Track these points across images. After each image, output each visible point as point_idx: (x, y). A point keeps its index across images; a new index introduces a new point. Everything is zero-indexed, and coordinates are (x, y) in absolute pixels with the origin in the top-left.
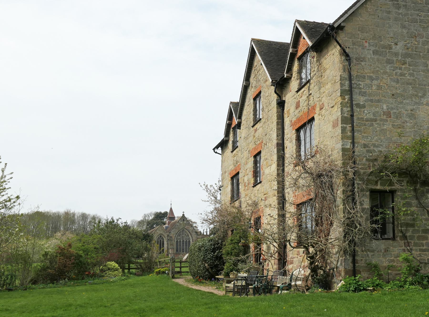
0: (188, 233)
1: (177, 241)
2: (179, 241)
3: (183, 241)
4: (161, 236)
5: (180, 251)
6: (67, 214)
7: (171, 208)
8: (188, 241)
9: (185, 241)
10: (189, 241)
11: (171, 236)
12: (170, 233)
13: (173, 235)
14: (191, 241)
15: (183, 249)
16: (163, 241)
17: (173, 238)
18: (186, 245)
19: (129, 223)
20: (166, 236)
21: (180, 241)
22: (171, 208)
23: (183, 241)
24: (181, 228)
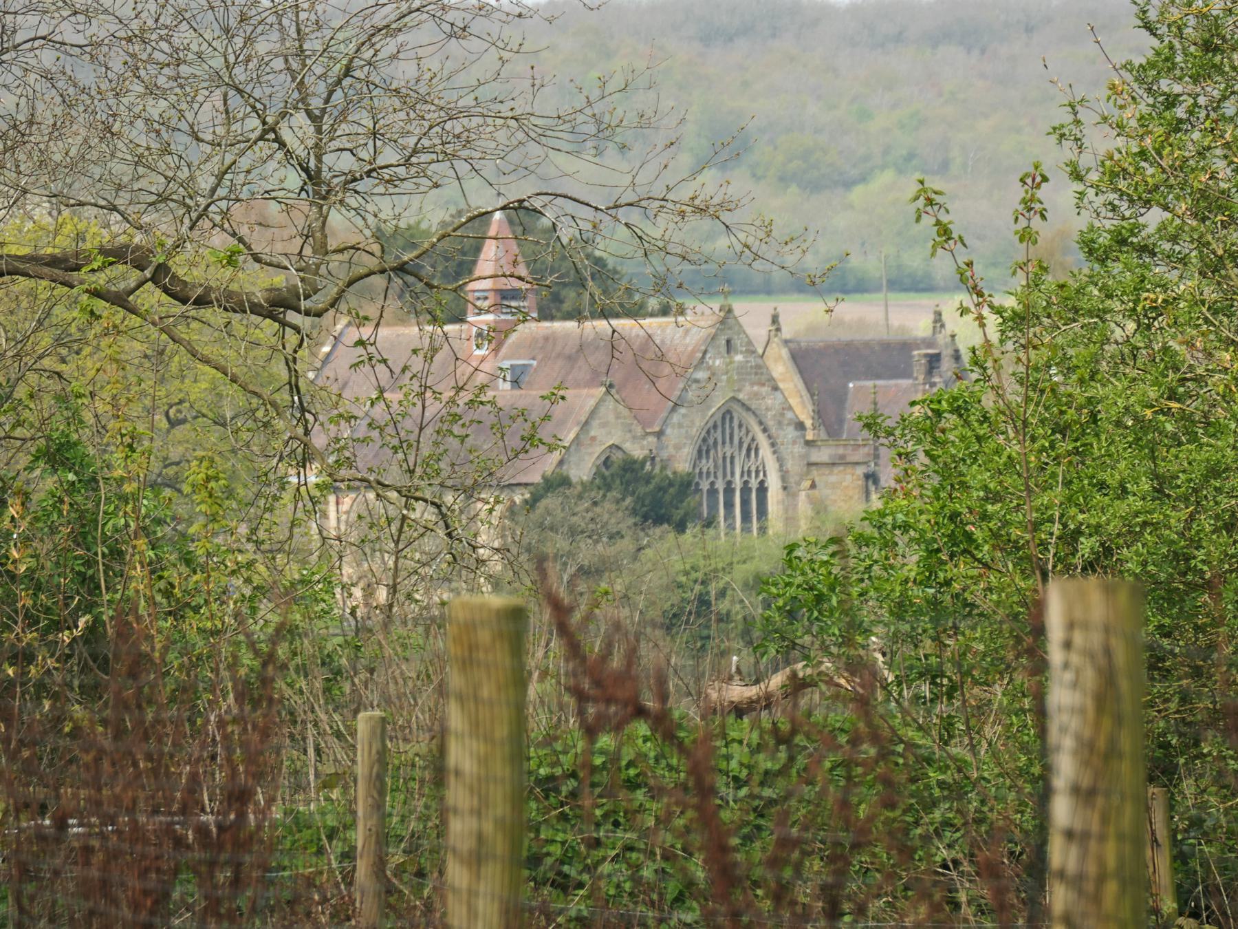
8: (754, 484)
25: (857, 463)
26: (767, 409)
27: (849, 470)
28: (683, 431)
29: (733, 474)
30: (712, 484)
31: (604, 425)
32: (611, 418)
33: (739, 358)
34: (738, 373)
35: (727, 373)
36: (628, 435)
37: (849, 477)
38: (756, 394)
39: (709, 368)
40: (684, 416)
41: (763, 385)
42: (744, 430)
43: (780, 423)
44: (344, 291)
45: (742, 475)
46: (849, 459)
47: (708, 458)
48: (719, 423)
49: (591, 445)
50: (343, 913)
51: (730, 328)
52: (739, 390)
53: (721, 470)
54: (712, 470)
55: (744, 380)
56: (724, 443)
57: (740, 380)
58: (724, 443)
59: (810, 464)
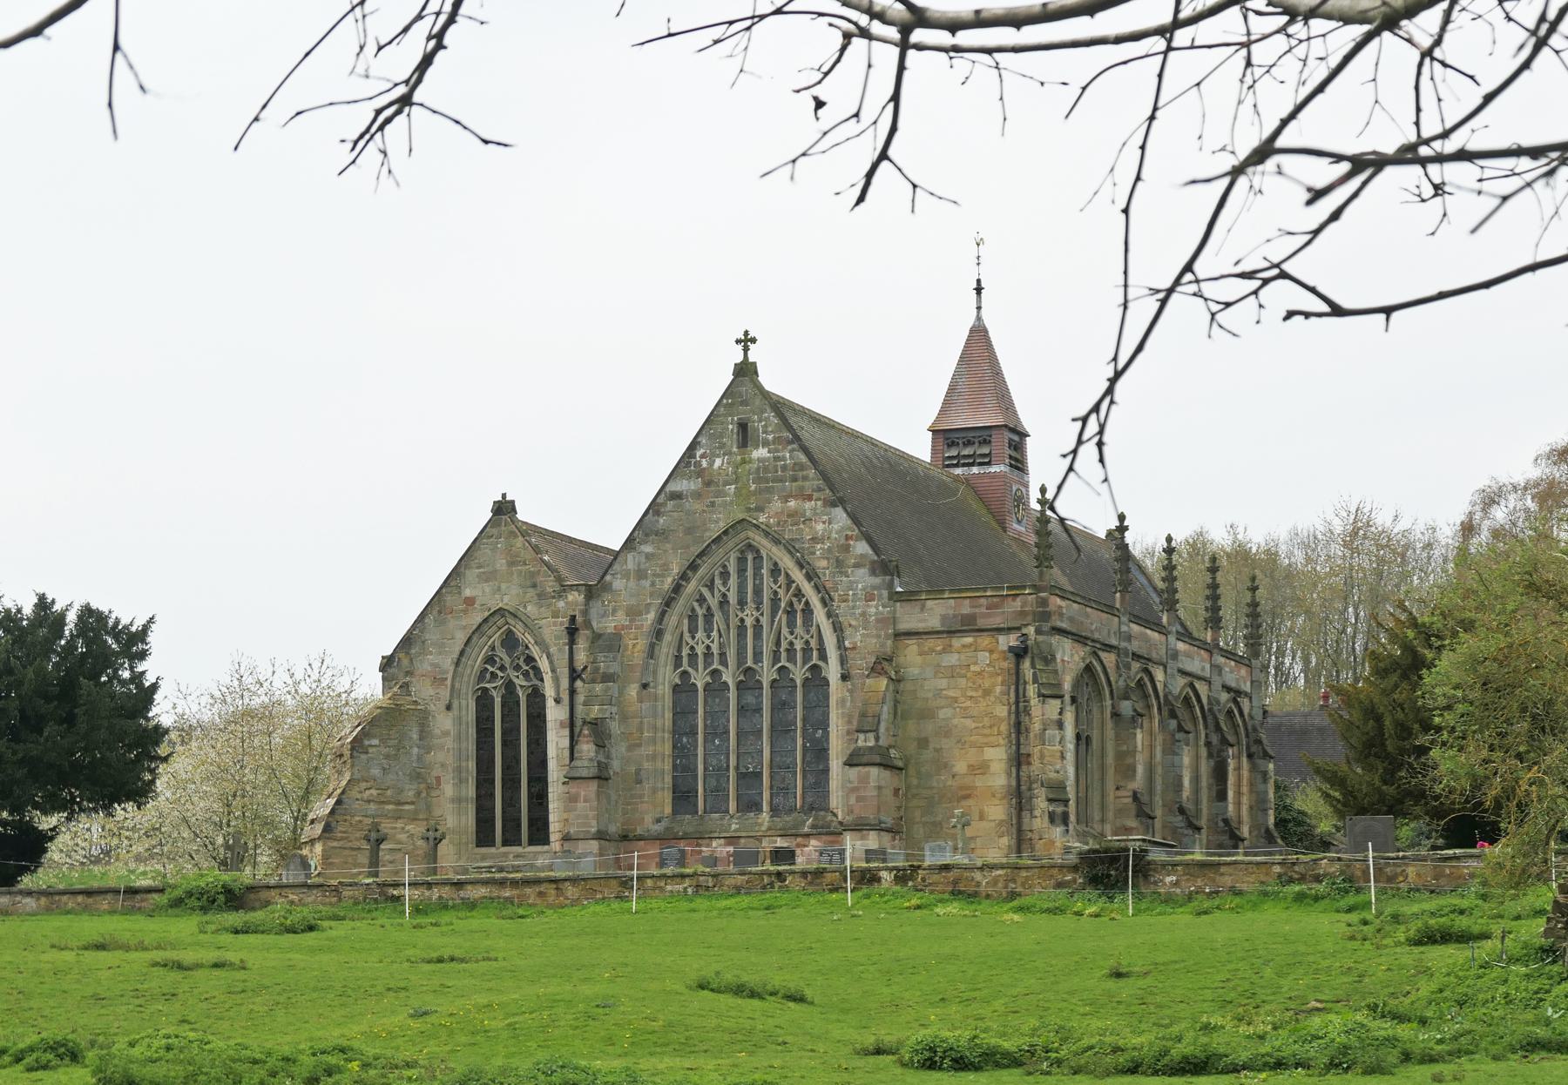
0: (798, 576)
1: (683, 689)
2: (700, 679)
3: (748, 682)
4: (510, 641)
5: (717, 795)
6: (1358, 532)
7: (979, 336)
8: (799, 673)
9: (767, 674)
10: (817, 681)
11: (609, 625)
12: (591, 593)
13: (633, 613)
14: (833, 671)
15: (749, 778)
16: (536, 697)
17: (636, 646)
18: (781, 730)
19: (1144, 540)
20: (553, 630)
21: (716, 688)
22: (979, 336)
23: (748, 682)
24: (718, 523)
25: (999, 630)
26: (814, 540)
27: (985, 641)
28: (646, 583)
29: (758, 657)
30: (715, 673)
31: (488, 577)
32: (501, 564)
33: (761, 453)
34: (758, 480)
35: (736, 481)
36: (531, 593)
37: (984, 657)
38: (793, 514)
39: (700, 473)
40: (648, 557)
41: (810, 498)
42: (782, 579)
43: (839, 563)
44: (1017, 713)
45: (776, 657)
46: (981, 623)
47: (708, 631)
48: (732, 568)
49: (465, 611)
50: (4, 912)
51: (744, 403)
52: (760, 509)
53: (1097, 784)
54: (715, 649)
55: (769, 490)
56: (742, 603)
57: (759, 491)
58: (742, 603)
59: (898, 635)
